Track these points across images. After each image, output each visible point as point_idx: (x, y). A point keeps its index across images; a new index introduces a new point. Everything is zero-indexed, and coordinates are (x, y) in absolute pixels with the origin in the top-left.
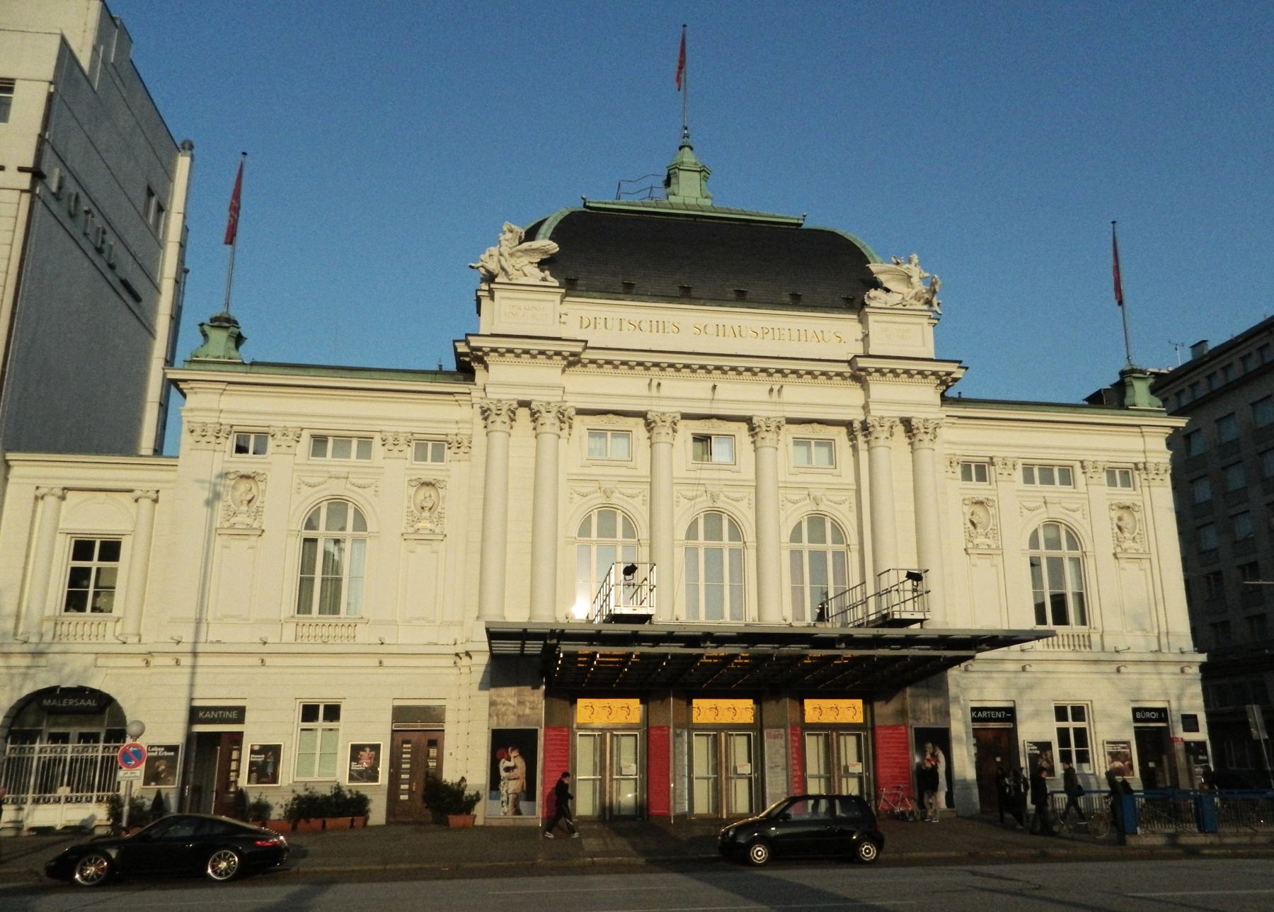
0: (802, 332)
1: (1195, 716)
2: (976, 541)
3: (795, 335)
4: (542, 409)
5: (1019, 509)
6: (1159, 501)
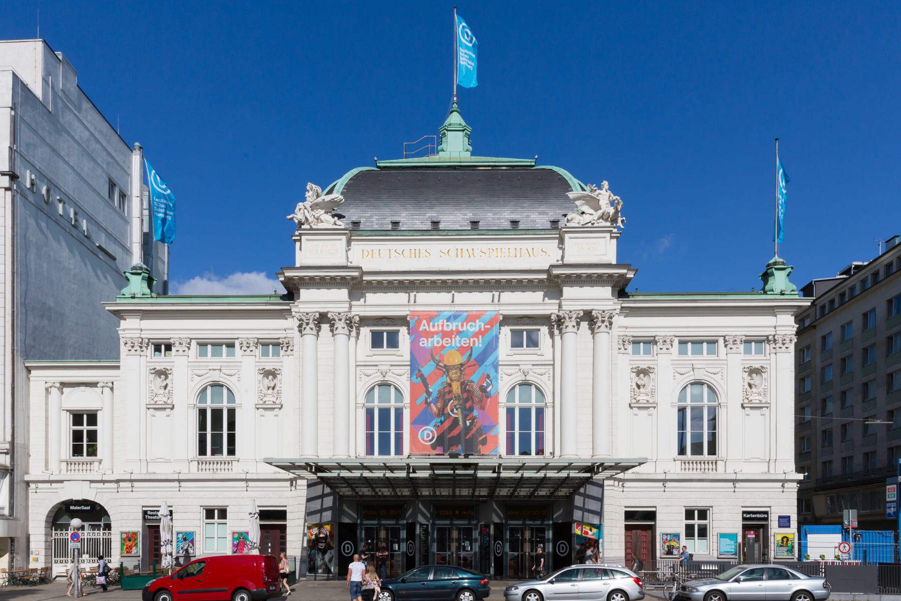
0: (459, 251)
1: (789, 517)
3: (512, 252)
4: (336, 318)
5: (670, 375)
6: (782, 367)
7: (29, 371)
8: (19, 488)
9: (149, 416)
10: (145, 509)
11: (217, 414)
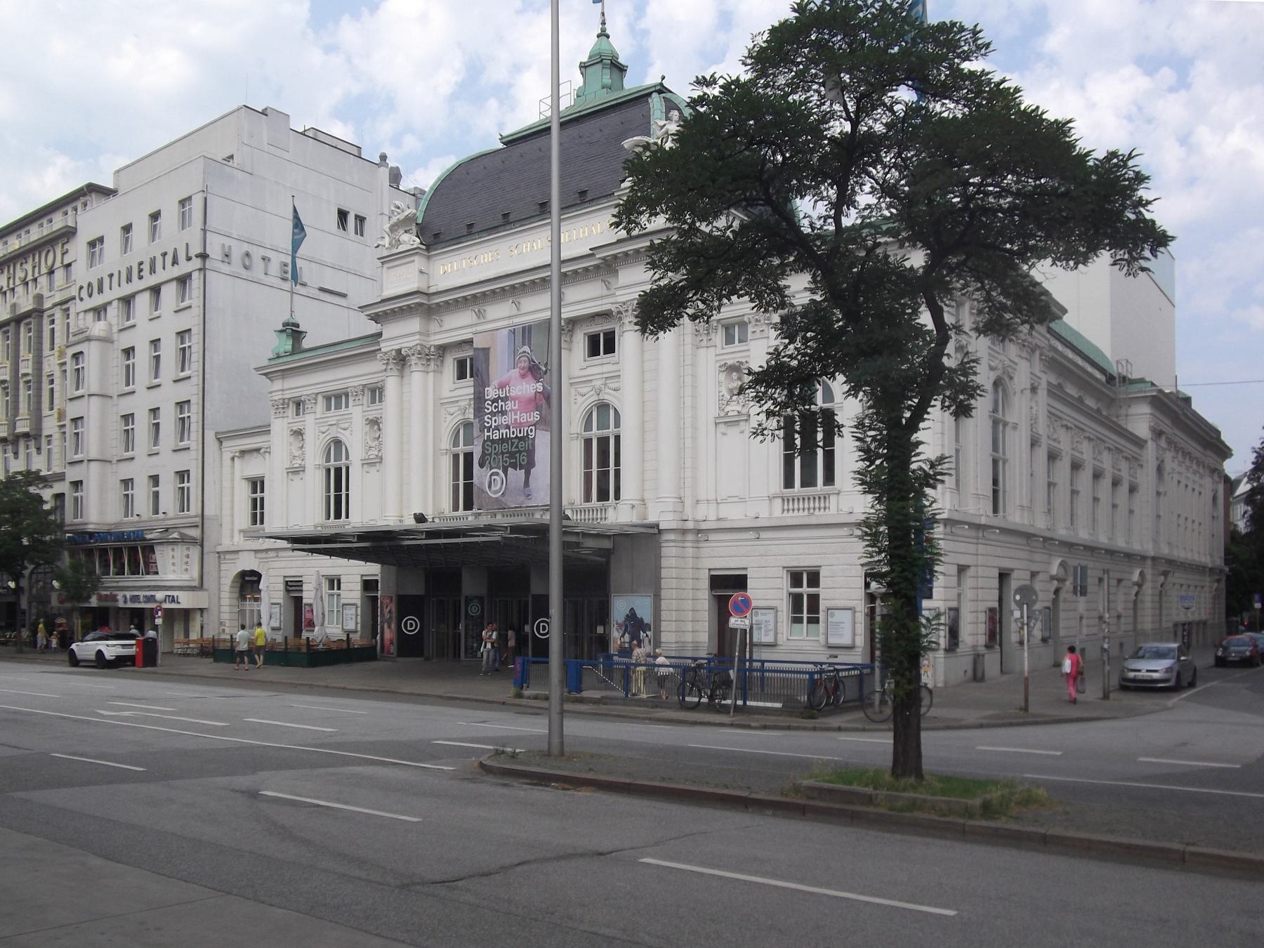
7: (221, 443)
8: (210, 560)
9: (719, 435)
10: (713, 573)
11: (604, 442)
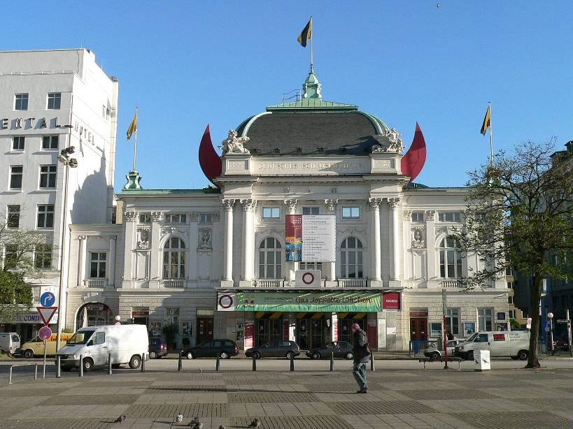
2: (202, 246)
11: (175, 255)
